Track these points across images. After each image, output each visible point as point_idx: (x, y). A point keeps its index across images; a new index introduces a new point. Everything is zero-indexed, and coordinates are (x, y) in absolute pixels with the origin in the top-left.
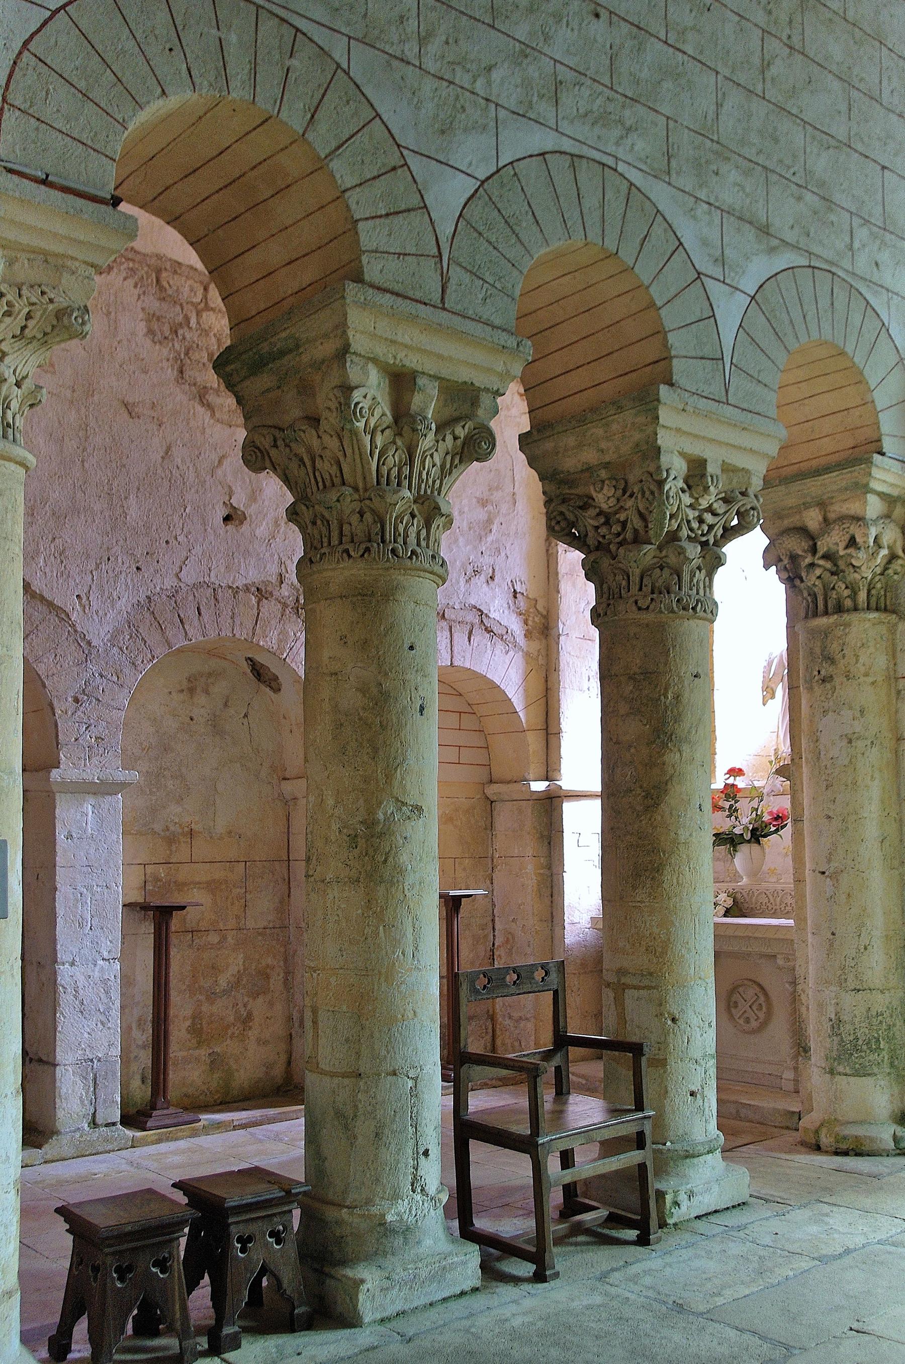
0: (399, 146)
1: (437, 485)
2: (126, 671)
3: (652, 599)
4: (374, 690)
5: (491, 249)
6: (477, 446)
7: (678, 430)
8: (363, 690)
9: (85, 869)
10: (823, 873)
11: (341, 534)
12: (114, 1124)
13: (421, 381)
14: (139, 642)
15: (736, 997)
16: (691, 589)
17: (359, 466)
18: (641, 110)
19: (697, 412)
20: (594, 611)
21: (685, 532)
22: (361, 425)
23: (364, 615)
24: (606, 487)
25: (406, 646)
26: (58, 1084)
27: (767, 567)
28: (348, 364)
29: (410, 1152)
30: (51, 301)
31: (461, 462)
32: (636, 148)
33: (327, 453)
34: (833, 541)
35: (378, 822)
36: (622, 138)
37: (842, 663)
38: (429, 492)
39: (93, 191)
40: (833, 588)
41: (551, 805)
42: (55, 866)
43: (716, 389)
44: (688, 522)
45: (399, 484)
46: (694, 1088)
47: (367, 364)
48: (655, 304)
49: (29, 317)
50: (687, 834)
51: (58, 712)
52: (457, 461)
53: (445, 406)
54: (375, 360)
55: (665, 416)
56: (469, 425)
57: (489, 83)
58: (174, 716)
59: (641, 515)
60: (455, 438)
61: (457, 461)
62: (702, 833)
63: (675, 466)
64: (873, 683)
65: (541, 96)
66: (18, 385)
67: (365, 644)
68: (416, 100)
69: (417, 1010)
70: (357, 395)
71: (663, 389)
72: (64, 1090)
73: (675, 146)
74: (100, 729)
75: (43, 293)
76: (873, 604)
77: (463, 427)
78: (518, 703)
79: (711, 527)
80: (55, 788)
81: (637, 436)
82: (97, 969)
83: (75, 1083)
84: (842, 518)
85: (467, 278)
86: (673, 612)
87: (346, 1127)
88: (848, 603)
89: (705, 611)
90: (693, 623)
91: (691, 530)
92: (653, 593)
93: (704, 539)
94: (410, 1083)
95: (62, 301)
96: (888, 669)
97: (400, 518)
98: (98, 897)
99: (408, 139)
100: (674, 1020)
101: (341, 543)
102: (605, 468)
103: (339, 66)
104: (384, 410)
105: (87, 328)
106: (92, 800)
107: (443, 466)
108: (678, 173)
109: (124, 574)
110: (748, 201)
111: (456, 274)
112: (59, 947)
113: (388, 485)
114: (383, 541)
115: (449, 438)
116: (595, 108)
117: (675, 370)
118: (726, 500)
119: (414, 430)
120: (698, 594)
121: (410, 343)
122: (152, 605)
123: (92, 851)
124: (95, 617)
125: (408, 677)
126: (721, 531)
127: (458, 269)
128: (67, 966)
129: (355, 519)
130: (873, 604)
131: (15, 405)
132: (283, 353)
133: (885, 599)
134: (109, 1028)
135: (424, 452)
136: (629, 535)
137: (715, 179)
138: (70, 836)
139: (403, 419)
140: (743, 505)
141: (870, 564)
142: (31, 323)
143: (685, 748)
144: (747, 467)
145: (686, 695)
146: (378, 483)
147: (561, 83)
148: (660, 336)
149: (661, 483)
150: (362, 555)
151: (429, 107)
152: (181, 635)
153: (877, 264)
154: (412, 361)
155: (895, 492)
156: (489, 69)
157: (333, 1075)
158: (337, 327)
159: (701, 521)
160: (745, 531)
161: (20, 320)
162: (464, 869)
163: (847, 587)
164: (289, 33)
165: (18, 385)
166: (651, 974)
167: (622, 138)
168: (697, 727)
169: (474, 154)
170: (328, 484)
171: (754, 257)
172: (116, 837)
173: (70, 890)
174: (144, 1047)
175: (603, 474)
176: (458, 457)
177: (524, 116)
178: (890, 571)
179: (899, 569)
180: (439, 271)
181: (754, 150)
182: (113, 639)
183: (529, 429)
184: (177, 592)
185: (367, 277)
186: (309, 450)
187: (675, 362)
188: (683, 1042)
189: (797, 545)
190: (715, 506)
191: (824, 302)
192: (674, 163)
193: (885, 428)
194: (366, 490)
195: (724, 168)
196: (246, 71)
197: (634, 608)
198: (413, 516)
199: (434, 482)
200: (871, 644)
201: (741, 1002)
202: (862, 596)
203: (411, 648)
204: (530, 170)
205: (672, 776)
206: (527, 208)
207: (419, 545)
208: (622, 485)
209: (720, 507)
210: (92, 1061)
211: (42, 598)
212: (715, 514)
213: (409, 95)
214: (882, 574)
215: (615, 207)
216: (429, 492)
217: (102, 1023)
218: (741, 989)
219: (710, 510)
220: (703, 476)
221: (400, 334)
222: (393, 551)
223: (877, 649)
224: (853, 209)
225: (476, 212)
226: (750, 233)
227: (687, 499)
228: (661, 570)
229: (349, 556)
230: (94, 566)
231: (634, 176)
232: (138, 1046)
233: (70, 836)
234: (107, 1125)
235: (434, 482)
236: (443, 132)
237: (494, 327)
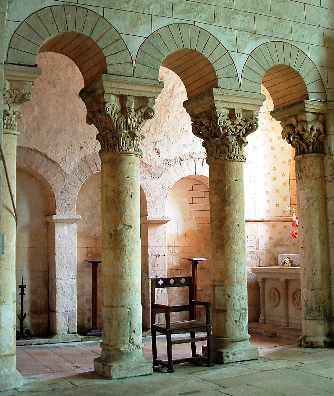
0: (119, 33)
1: (137, 127)
2: (78, 182)
3: (220, 156)
4: (117, 191)
5: (150, 56)
7: (222, 101)
8: (113, 190)
9: (64, 248)
10: (302, 248)
11: (108, 144)
12: (75, 333)
13: (128, 98)
14: (82, 172)
15: (295, 296)
16: (233, 152)
17: (111, 124)
18: (204, 6)
19: (228, 95)
21: (230, 133)
22: (110, 113)
23: (113, 168)
24: (205, 119)
25: (126, 177)
26: (57, 318)
27: (283, 138)
28: (104, 97)
29: (129, 331)
30: (21, 92)
31: (144, 119)
32: (202, 17)
34: (299, 129)
35: (118, 230)
36: (196, 15)
37: (305, 172)
38: (134, 129)
39: (31, 64)
40: (302, 145)
42: (55, 247)
43: (236, 87)
44: (231, 130)
45: (123, 129)
46: (236, 319)
47: (110, 96)
48: (210, 63)
49: (16, 97)
50: (233, 234)
51: (56, 196)
52: (143, 119)
53: (138, 103)
54: (113, 94)
55: (216, 98)
56: (146, 108)
57: (149, 9)
58: (97, 196)
60: (142, 113)
61: (143, 119)
62: (239, 234)
64: (315, 179)
65: (167, 9)
66: (14, 114)
67: (114, 177)
68: (124, 20)
69: (130, 288)
70: (107, 105)
71: (214, 90)
72: (59, 320)
73: (217, 14)
74: (69, 202)
75: (19, 91)
76: (315, 151)
77: (144, 109)
79: (240, 130)
80: (54, 221)
81: (210, 104)
82: (69, 281)
83: (62, 318)
85: (141, 67)
86: (226, 159)
87: (110, 322)
88: (306, 150)
89: (238, 159)
90: (234, 163)
91: (233, 132)
92: (220, 153)
93: (238, 134)
94: (128, 310)
95: (24, 92)
96: (321, 173)
97: (124, 138)
98: (69, 257)
99: (122, 31)
100: (229, 297)
101: (107, 147)
102: (204, 113)
103: (100, 16)
104: (118, 106)
105: (30, 98)
106: (67, 225)
107: (138, 122)
108: (218, 22)
109: (77, 150)
110: (247, 25)
111: (138, 66)
112: (56, 273)
113: (120, 129)
114: (119, 146)
115: (139, 113)
116: (187, 8)
117: (219, 83)
118: (245, 121)
119: (127, 112)
120: (235, 153)
121: (123, 88)
122: (86, 159)
123: (67, 242)
124: (67, 165)
125: (127, 186)
126: (245, 131)
127: (138, 65)
128: (59, 280)
129: (111, 139)
130: (315, 151)
131: (13, 119)
132: (92, 92)
133: (320, 149)
134: (73, 301)
135: (131, 118)
136: (213, 135)
137: (233, 20)
138: (60, 237)
139: (124, 111)
140: (251, 122)
141: (310, 137)
142: (16, 99)
143: (231, 205)
144: (251, 110)
145: (232, 187)
146: (117, 128)
147: (174, 3)
148: (214, 72)
149: (217, 118)
150: (112, 150)
151: (129, 21)
152: (96, 169)
153: (303, 36)
154: (125, 93)
155: (318, 112)
156: (149, 6)
157: (106, 307)
158: (101, 86)
159: (236, 128)
160: (253, 131)
161: (14, 98)
162: (207, 250)
163: (305, 145)
164: (85, 11)
165: (14, 114)
166: (222, 281)
167: (196, 15)
168: (236, 198)
169: (144, 31)
170: (104, 129)
171: (249, 42)
172: (75, 237)
173: (60, 255)
174: (88, 310)
175: (204, 115)
176: (143, 118)
177: (161, 16)
178: (320, 139)
179: (322, 138)
180: (132, 66)
181: (249, 9)
182: (73, 172)
183: (187, 99)
184: (94, 154)
185: (108, 72)
186: (100, 119)
187: (219, 80)
188: (232, 304)
189: (289, 130)
190: (241, 123)
192: (217, 19)
193: (309, 91)
194: (114, 131)
195: (237, 16)
196: (73, 24)
197: (214, 159)
198: (128, 137)
199: (135, 126)
200: (314, 165)
201: (297, 298)
202: (311, 148)
203: (128, 177)
205: (227, 215)
206: (163, 42)
207: (130, 146)
208: (210, 118)
209: (243, 123)
210: (68, 311)
211: (51, 160)
212: (241, 126)
213: (122, 19)
214: (317, 140)
216: (134, 129)
217: (71, 299)
218: (297, 293)
219: (240, 124)
220: (234, 114)
221: (120, 86)
222: (121, 149)
223: (316, 167)
224: (292, 20)
225: (144, 47)
226: (248, 35)
227: (229, 122)
228: (223, 146)
229: (109, 151)
230: (67, 148)
231: (201, 26)
232: (86, 309)
233: (60, 237)
234: (73, 333)
235: (135, 126)
236: (133, 27)
237: (151, 79)
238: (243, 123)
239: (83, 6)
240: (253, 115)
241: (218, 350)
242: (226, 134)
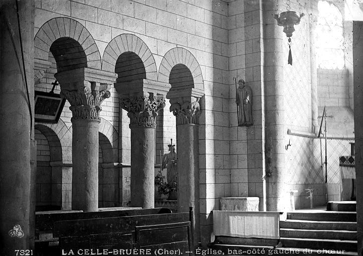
6: (106, 96)
20: (130, 125)
21: (149, 109)
33: (78, 98)
41: (120, 167)
59: (140, 105)
63: (146, 95)
70: (85, 88)
78: (111, 140)
79: (155, 107)
84: (186, 101)
139: (93, 92)
159: (152, 106)
191: (180, 55)
204: (118, 39)
209: (157, 103)
212: (156, 104)
215: (135, 42)
219: (154, 103)
231: (138, 35)
238: (157, 103)
239: (74, 19)
240: (163, 98)
241: (67, 104)
242: (147, 110)
